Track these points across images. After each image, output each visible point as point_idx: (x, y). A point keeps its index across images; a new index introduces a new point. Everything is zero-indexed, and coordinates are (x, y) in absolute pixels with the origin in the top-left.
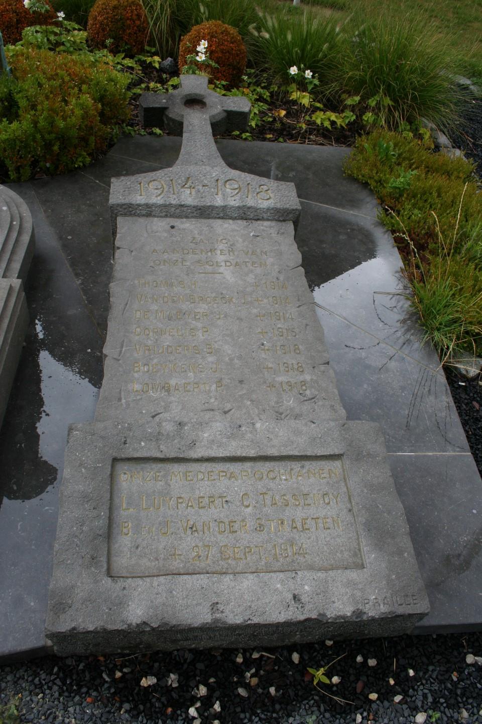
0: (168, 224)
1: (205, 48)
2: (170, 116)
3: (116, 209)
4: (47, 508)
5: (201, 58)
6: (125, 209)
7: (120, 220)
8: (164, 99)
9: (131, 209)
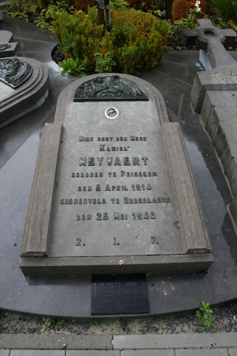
0: (231, 94)
1: (198, 5)
2: (200, 40)
3: (206, 87)
4: (226, 230)
5: (198, 10)
6: (209, 87)
7: (208, 92)
8: (195, 32)
9: (212, 87)
